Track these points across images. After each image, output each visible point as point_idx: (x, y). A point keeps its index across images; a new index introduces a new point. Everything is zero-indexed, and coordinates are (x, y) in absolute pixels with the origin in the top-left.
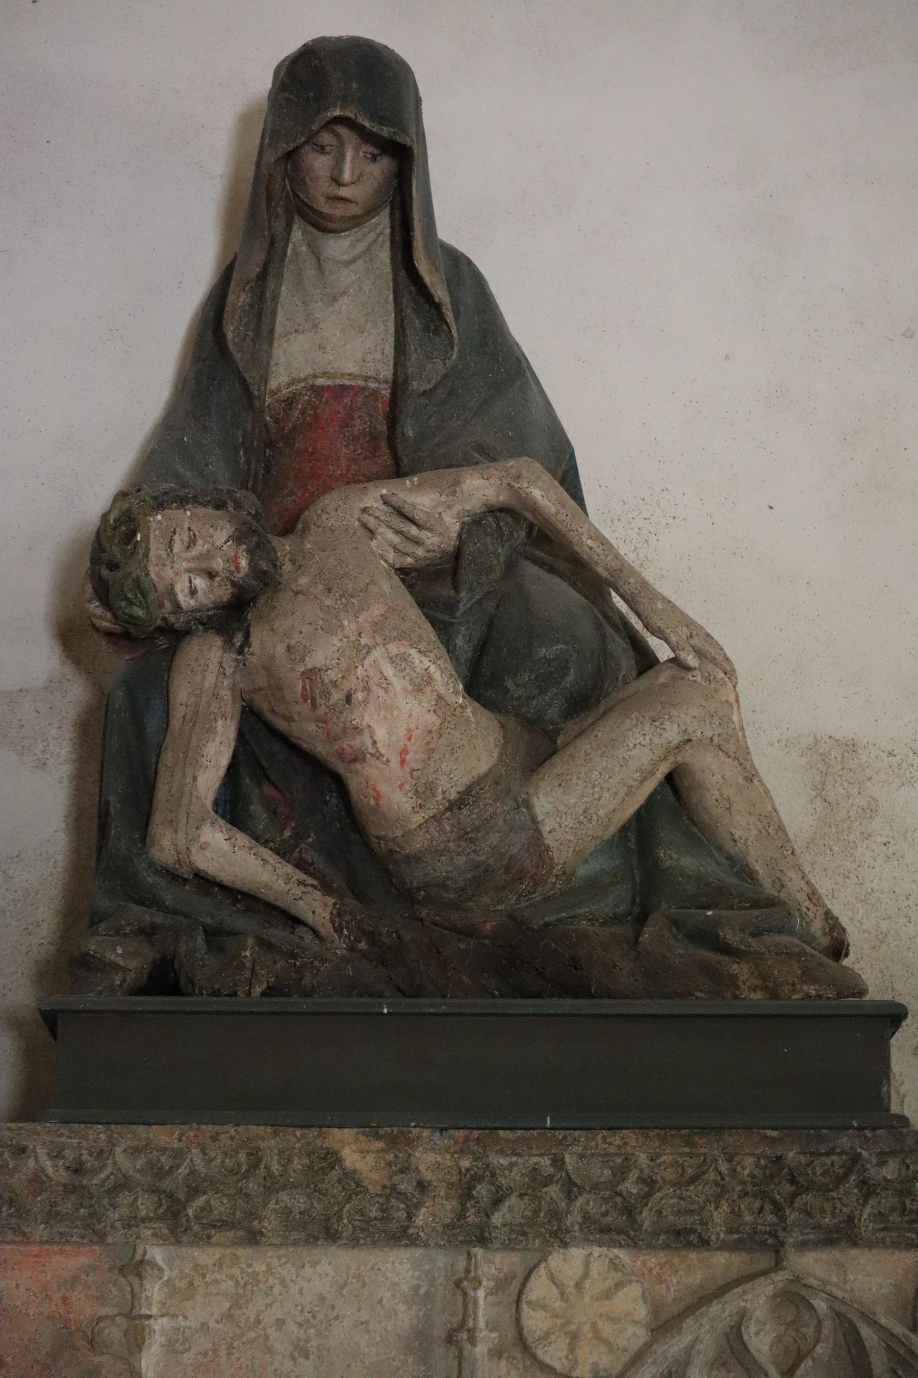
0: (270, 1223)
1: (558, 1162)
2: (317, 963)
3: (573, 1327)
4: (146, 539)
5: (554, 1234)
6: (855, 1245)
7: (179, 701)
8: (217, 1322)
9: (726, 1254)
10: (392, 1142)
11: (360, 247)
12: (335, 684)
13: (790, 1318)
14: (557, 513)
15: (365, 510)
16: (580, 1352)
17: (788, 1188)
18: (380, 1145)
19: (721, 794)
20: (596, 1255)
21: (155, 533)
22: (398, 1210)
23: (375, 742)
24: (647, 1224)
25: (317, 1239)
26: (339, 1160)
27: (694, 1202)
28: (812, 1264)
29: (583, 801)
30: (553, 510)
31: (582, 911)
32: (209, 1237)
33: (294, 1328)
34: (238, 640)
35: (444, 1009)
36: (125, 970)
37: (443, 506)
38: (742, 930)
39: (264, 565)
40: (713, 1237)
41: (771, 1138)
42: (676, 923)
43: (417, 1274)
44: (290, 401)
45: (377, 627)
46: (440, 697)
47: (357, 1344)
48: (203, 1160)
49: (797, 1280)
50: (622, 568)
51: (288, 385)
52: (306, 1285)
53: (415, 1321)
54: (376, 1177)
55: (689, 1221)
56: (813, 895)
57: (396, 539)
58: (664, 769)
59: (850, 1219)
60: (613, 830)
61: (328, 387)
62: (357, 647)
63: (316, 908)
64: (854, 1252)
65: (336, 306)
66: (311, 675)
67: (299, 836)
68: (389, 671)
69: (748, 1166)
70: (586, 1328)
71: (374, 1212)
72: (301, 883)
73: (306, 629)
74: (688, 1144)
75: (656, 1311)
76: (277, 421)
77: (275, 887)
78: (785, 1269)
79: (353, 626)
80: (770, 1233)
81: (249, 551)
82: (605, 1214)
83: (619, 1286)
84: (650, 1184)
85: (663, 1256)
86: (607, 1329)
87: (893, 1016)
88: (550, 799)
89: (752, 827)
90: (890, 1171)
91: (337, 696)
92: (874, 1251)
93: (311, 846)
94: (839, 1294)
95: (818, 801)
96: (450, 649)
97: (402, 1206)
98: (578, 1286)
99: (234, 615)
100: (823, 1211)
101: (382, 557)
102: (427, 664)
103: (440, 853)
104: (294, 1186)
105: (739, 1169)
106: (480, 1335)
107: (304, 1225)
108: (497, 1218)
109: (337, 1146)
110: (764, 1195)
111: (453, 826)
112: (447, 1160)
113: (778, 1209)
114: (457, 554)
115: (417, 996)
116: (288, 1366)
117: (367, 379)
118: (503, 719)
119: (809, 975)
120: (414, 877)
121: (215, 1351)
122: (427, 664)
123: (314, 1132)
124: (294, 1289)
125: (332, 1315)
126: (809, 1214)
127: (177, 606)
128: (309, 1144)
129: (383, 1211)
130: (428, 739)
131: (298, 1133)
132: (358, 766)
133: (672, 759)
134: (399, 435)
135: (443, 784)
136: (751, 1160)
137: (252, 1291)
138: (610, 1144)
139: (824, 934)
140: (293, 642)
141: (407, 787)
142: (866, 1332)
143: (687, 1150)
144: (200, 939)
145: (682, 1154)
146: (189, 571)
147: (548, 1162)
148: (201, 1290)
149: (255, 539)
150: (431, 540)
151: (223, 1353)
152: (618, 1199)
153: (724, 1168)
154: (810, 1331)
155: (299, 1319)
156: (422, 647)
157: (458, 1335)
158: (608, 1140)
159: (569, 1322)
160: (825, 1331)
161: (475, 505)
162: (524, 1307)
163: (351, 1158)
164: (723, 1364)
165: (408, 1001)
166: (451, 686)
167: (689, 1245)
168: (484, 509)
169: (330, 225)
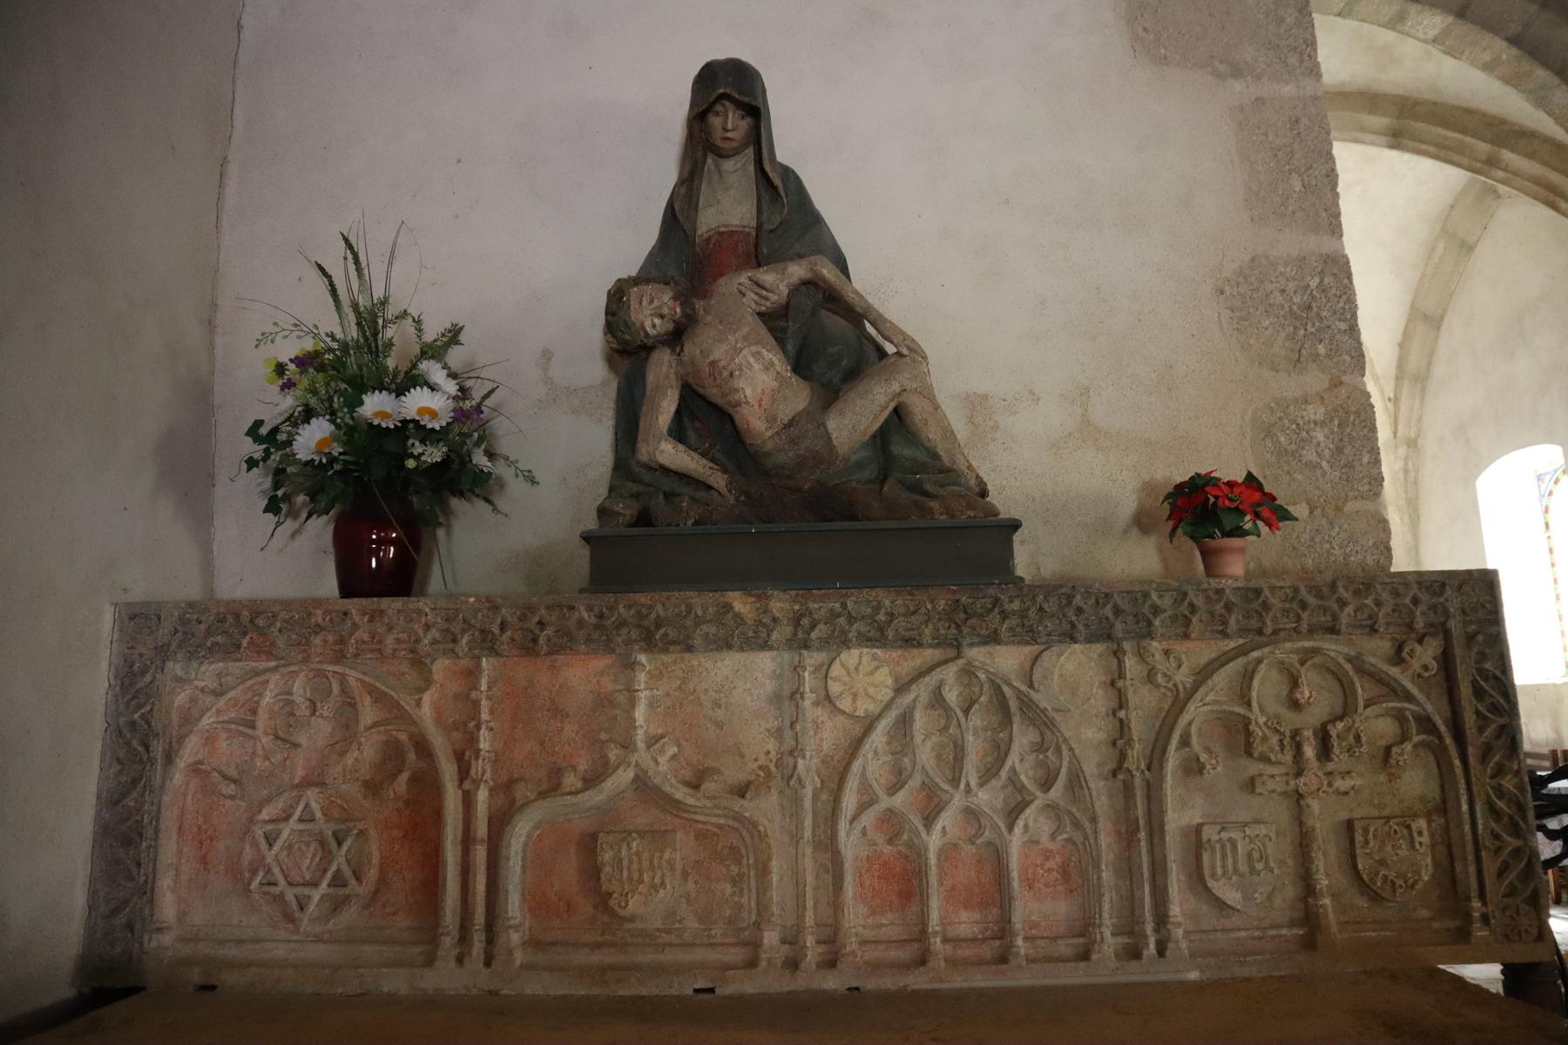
0: (697, 641)
1: (844, 605)
10: (759, 597)
17: (962, 616)
21: (633, 296)
28: (976, 654)
29: (852, 423)
37: (780, 281)
44: (708, 240)
45: (745, 338)
49: (969, 663)
50: (869, 308)
56: (970, 467)
58: (891, 408)
59: (996, 631)
62: (735, 349)
63: (718, 480)
66: (713, 364)
67: (712, 446)
68: (751, 360)
71: (751, 634)
75: (896, 680)
83: (877, 668)
84: (891, 615)
85: (900, 652)
86: (872, 690)
87: (1015, 525)
90: (1016, 605)
91: (725, 374)
98: (856, 669)
99: (677, 336)
108: (813, 635)
110: (950, 620)
113: (958, 627)
116: (710, 713)
119: (970, 506)
127: (647, 334)
134: (758, 249)
142: (1006, 689)
144: (661, 497)
150: (774, 298)
154: (977, 689)
157: (796, 695)
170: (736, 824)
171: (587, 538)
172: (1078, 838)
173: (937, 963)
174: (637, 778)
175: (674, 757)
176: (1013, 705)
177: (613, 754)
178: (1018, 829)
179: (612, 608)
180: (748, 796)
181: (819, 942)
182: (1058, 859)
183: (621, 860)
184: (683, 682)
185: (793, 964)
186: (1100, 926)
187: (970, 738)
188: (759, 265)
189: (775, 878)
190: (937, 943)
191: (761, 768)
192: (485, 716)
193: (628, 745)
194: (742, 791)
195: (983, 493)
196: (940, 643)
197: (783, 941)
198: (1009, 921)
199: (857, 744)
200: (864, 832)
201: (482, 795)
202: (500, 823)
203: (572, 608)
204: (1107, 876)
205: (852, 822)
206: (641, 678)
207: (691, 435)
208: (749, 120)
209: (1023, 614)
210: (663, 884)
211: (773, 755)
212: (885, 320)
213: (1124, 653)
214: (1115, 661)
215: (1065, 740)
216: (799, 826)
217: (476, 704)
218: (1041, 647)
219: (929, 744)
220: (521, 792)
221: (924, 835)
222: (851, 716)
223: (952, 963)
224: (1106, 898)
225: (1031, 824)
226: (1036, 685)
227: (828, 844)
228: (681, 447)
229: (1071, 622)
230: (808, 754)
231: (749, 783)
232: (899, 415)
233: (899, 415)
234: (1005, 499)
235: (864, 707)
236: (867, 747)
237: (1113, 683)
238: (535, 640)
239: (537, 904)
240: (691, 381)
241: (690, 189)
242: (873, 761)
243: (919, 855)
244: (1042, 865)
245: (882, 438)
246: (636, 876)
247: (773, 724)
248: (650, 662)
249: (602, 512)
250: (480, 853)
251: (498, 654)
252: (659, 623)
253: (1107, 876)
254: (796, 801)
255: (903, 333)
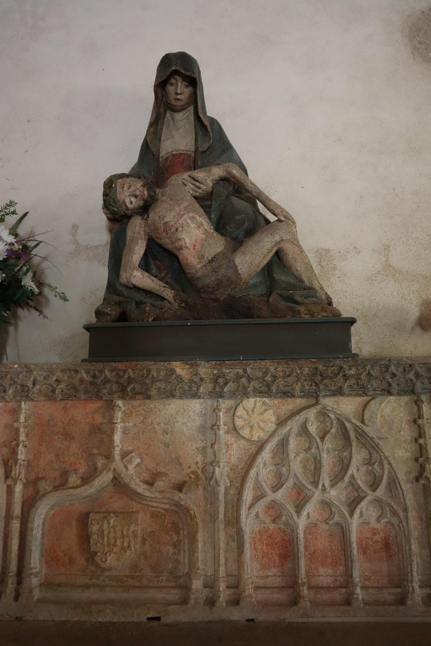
0: (153, 392)
1: (245, 371)
2: (169, 311)
3: (251, 424)
4: (116, 186)
5: (244, 394)
6: (342, 396)
7: (128, 235)
8: (139, 424)
9: (300, 399)
10: (192, 365)
11: (185, 116)
12: (173, 226)
13: (321, 420)
14: (240, 177)
15: (183, 179)
16: (254, 432)
17: (319, 378)
18: (188, 367)
19: (293, 257)
20: (258, 400)
21: (118, 184)
22: (194, 387)
23: (185, 243)
24: (274, 391)
25: (169, 397)
26: (175, 372)
27: (289, 383)
28: (328, 402)
29: (251, 260)
30: (239, 176)
31: (251, 293)
32: (135, 397)
33: (163, 425)
34: (146, 217)
35: (207, 323)
36: (111, 315)
37: (208, 177)
38: (301, 297)
39: (152, 193)
40: (296, 394)
41: (314, 361)
42: (280, 295)
43: (202, 407)
44: (167, 159)
45: (185, 208)
46: (205, 230)
47: (183, 430)
48: (133, 373)
49: (324, 408)
50: (261, 193)
51: (166, 155)
52: (166, 411)
53: (201, 422)
54: (187, 377)
55: (288, 389)
56: (321, 288)
57: (193, 187)
58: (275, 250)
59: (341, 388)
60: (260, 269)
61: (177, 154)
62: (179, 214)
63: (168, 294)
64: (342, 398)
65: (179, 131)
66: (166, 224)
67: (166, 275)
68: (189, 222)
69: (306, 371)
70: (256, 424)
71: (187, 388)
72: (164, 287)
73: (164, 211)
74: (287, 364)
75: (278, 419)
76: (163, 166)
77: (156, 288)
78: (320, 404)
79: (178, 209)
80: (314, 393)
81: (147, 189)
82: (261, 387)
83: (266, 410)
84: (275, 377)
85: (280, 400)
86: (262, 425)
87: (352, 321)
88: (240, 259)
89: (303, 267)
90: (353, 372)
91: (173, 229)
92: (348, 397)
93: (169, 277)
94: (338, 412)
95: (319, 266)
96: (210, 219)
97: (195, 386)
98: (253, 411)
99: (145, 209)
100: (331, 385)
101: (189, 192)
102: (201, 220)
103: (206, 276)
104: (161, 380)
105: (303, 372)
106: (221, 427)
107: (164, 393)
108: (226, 389)
109: (174, 367)
110: (312, 380)
111: (210, 268)
112: (209, 371)
113: (317, 385)
114: (212, 192)
115: (200, 319)
116: (161, 437)
117: (187, 151)
118: (226, 238)
119: (323, 310)
120: (200, 284)
121: (139, 433)
122: (201, 220)
123: (167, 363)
124: (163, 413)
125: (175, 420)
126: (327, 386)
127: (127, 207)
128: (165, 367)
129: (190, 388)
130: (202, 242)
131: (162, 364)
132: (181, 251)
133: (277, 246)
134: (196, 161)
135: (207, 255)
136: (307, 369)
137: (150, 414)
138: (261, 365)
139: (326, 299)
140: (160, 215)
141: (196, 256)
142: (347, 425)
143: (286, 366)
144: (133, 305)
145: (285, 367)
146: (129, 196)
147: (242, 371)
148: (134, 414)
149: (149, 186)
150: (203, 187)
151: (141, 434)
152: (265, 382)
153: (299, 372)
154: (329, 424)
155: (165, 422)
156: (199, 215)
157: (215, 427)
158: (261, 363)
159: (250, 422)
160: (334, 425)
161: (216, 177)
162: (236, 418)
163: (179, 371)
164: (301, 435)
165: (197, 321)
166: (209, 227)
167: (288, 397)
168: (219, 178)
169: (176, 108)
170: (176, 509)
171: (87, 328)
172: (395, 521)
173: (305, 604)
174: (115, 478)
175: (138, 465)
176: (352, 434)
177: (100, 462)
178: (356, 516)
179: (101, 371)
180: (184, 490)
181: (228, 587)
182: (382, 535)
183: (103, 531)
184: (145, 418)
185: (211, 602)
186: (412, 582)
187: (325, 455)
188: (195, 169)
189: (200, 545)
190: (305, 591)
191: (192, 472)
192: (22, 437)
193: (109, 457)
194: (179, 487)
195: (330, 303)
196: (305, 395)
197: (205, 586)
198: (352, 577)
199: (253, 458)
200: (257, 516)
201: (18, 488)
202: (29, 505)
203: (77, 371)
204: (415, 547)
205: (250, 508)
206: (119, 415)
207: (154, 270)
208: (190, 88)
209: (358, 378)
210: (129, 547)
211: (200, 465)
212: (271, 200)
213: (422, 402)
214: (416, 407)
215: (386, 457)
216: (216, 512)
217: (17, 431)
218: (369, 398)
219: (299, 459)
220: (43, 486)
221: (295, 518)
222: (249, 440)
223: (315, 604)
224: (415, 563)
225: (364, 510)
226: (366, 422)
227: (234, 522)
228: (146, 274)
229: (388, 383)
230: (222, 464)
231: (185, 482)
232: (279, 255)
233: (279, 255)
234: (345, 306)
235: (257, 435)
236: (259, 461)
237: (415, 421)
238: (53, 391)
239: (51, 557)
240: (154, 236)
241: (156, 129)
242: (263, 469)
243: (292, 531)
244: (372, 539)
245: (268, 270)
246: (112, 542)
247: (200, 444)
248: (124, 405)
249: (98, 313)
250: (16, 525)
251: (31, 400)
252: (130, 381)
253: (415, 547)
254: (214, 494)
255: (281, 208)
